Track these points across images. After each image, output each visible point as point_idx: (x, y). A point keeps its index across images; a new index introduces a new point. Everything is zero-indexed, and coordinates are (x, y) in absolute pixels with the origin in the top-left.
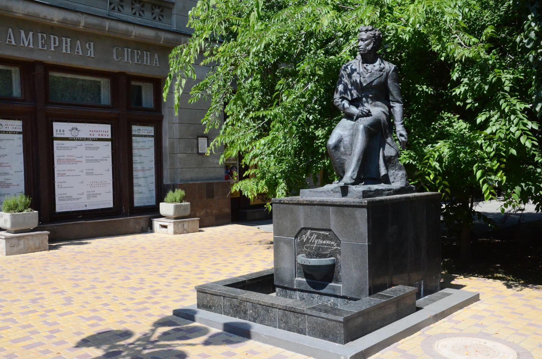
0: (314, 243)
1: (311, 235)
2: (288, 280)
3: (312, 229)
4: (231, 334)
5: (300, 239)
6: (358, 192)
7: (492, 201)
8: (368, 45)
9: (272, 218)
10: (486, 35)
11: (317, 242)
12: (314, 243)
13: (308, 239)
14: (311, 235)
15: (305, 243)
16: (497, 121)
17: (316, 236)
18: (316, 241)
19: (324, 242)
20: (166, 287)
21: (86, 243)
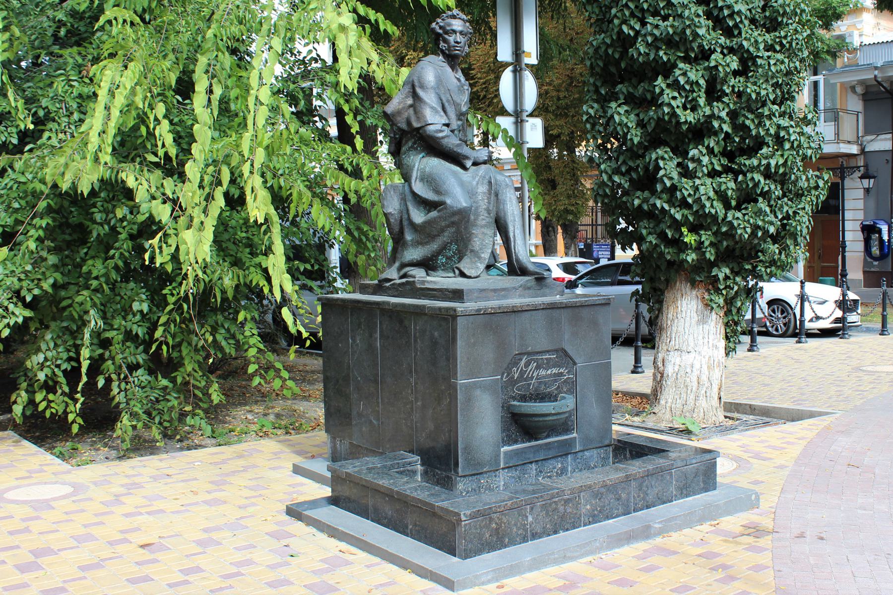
0: (532, 377)
1: (527, 364)
2: (487, 458)
3: (529, 354)
4: (664, 546)
5: (507, 377)
6: (470, 300)
7: (215, 197)
9: (612, 337)
10: (381, 142)
11: (538, 375)
12: (532, 377)
13: (522, 373)
14: (527, 364)
15: (516, 382)
16: (712, 163)
17: (535, 364)
18: (535, 374)
19: (549, 372)
20: (178, 497)
21: (856, 336)
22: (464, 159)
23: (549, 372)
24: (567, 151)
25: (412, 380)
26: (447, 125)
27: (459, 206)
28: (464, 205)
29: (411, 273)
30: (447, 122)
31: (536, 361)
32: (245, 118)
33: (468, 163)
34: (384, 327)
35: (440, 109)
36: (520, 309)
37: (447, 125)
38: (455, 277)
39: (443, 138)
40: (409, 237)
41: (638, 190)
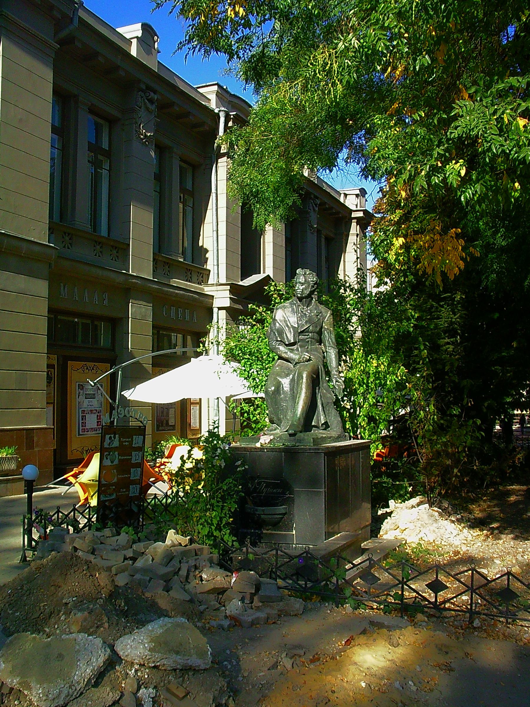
8: (306, 289)
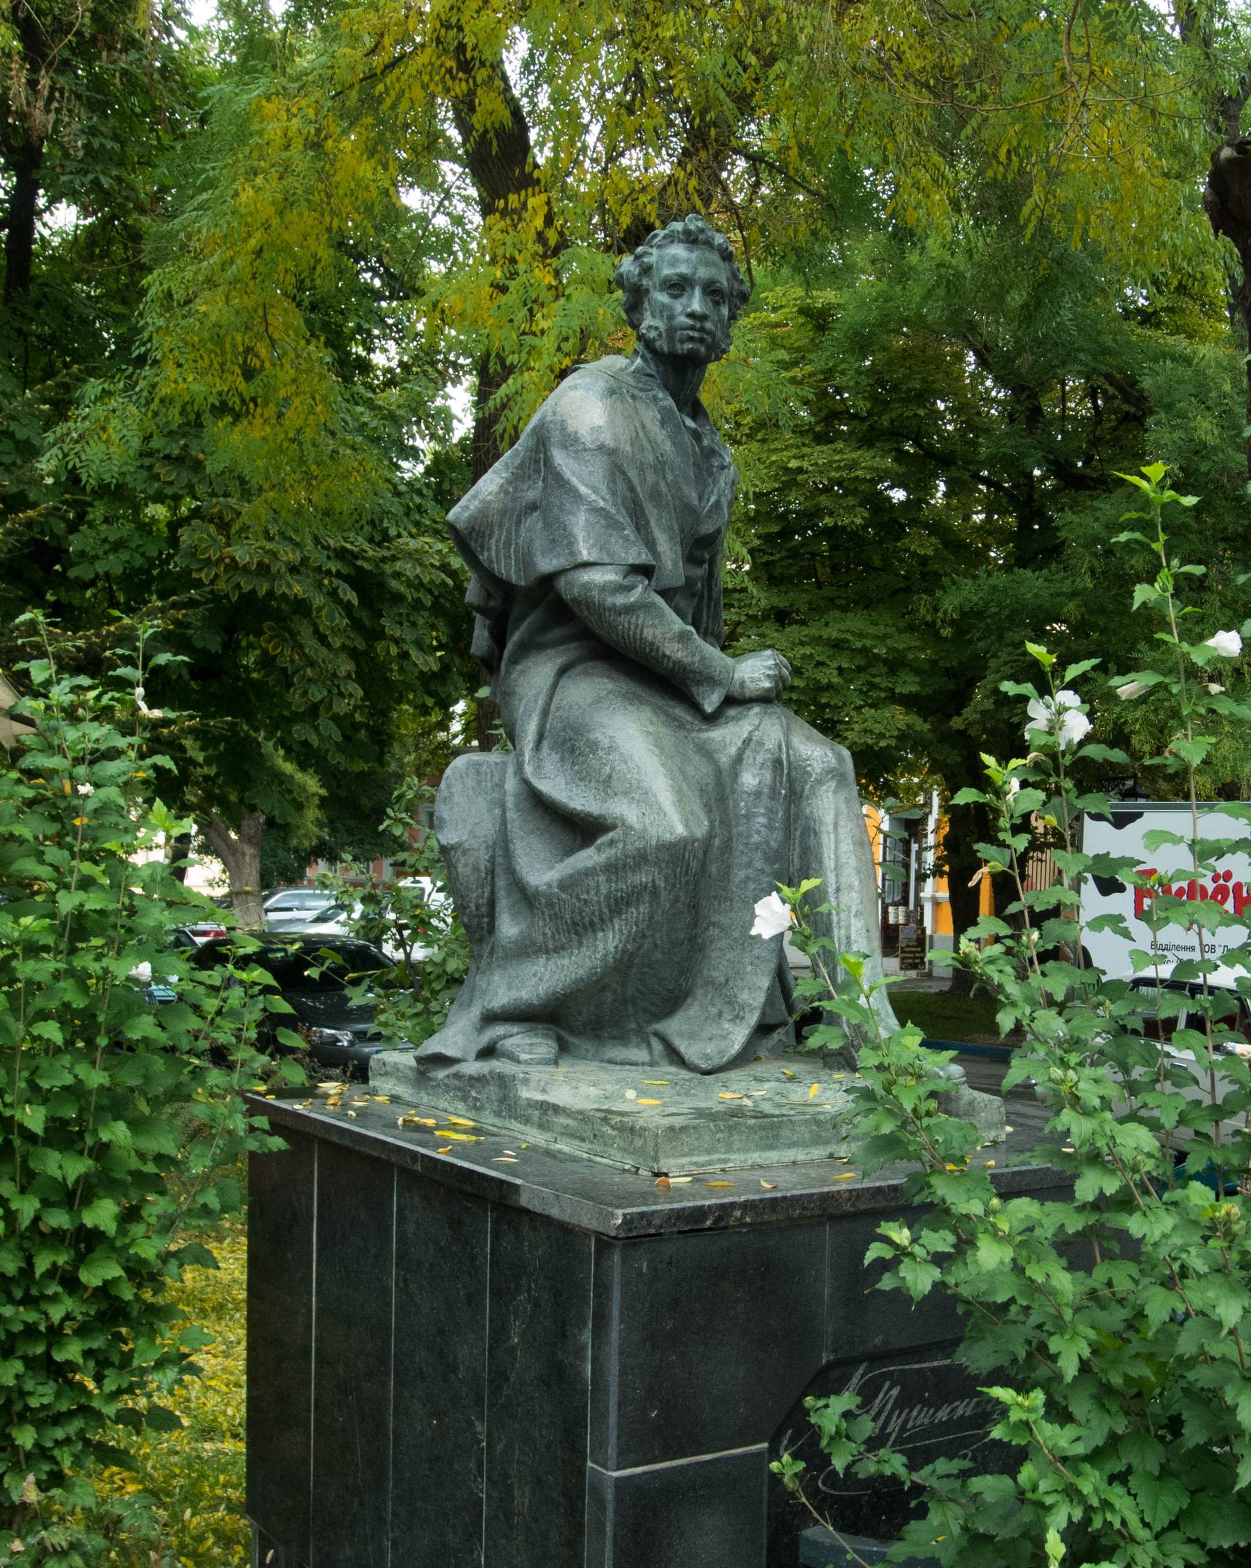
11: (903, 1428)
17: (895, 1392)
19: (943, 1414)
22: (699, 683)
23: (943, 1414)
24: (756, 511)
25: (481, 1428)
26: (645, 571)
27: (668, 837)
28: (680, 830)
29: (508, 1044)
30: (644, 558)
31: (895, 1379)
32: (267, 552)
33: (710, 703)
34: (411, 1228)
35: (623, 518)
36: (848, 1207)
37: (645, 571)
38: (652, 1064)
39: (629, 609)
40: (509, 928)
41: (387, 680)
